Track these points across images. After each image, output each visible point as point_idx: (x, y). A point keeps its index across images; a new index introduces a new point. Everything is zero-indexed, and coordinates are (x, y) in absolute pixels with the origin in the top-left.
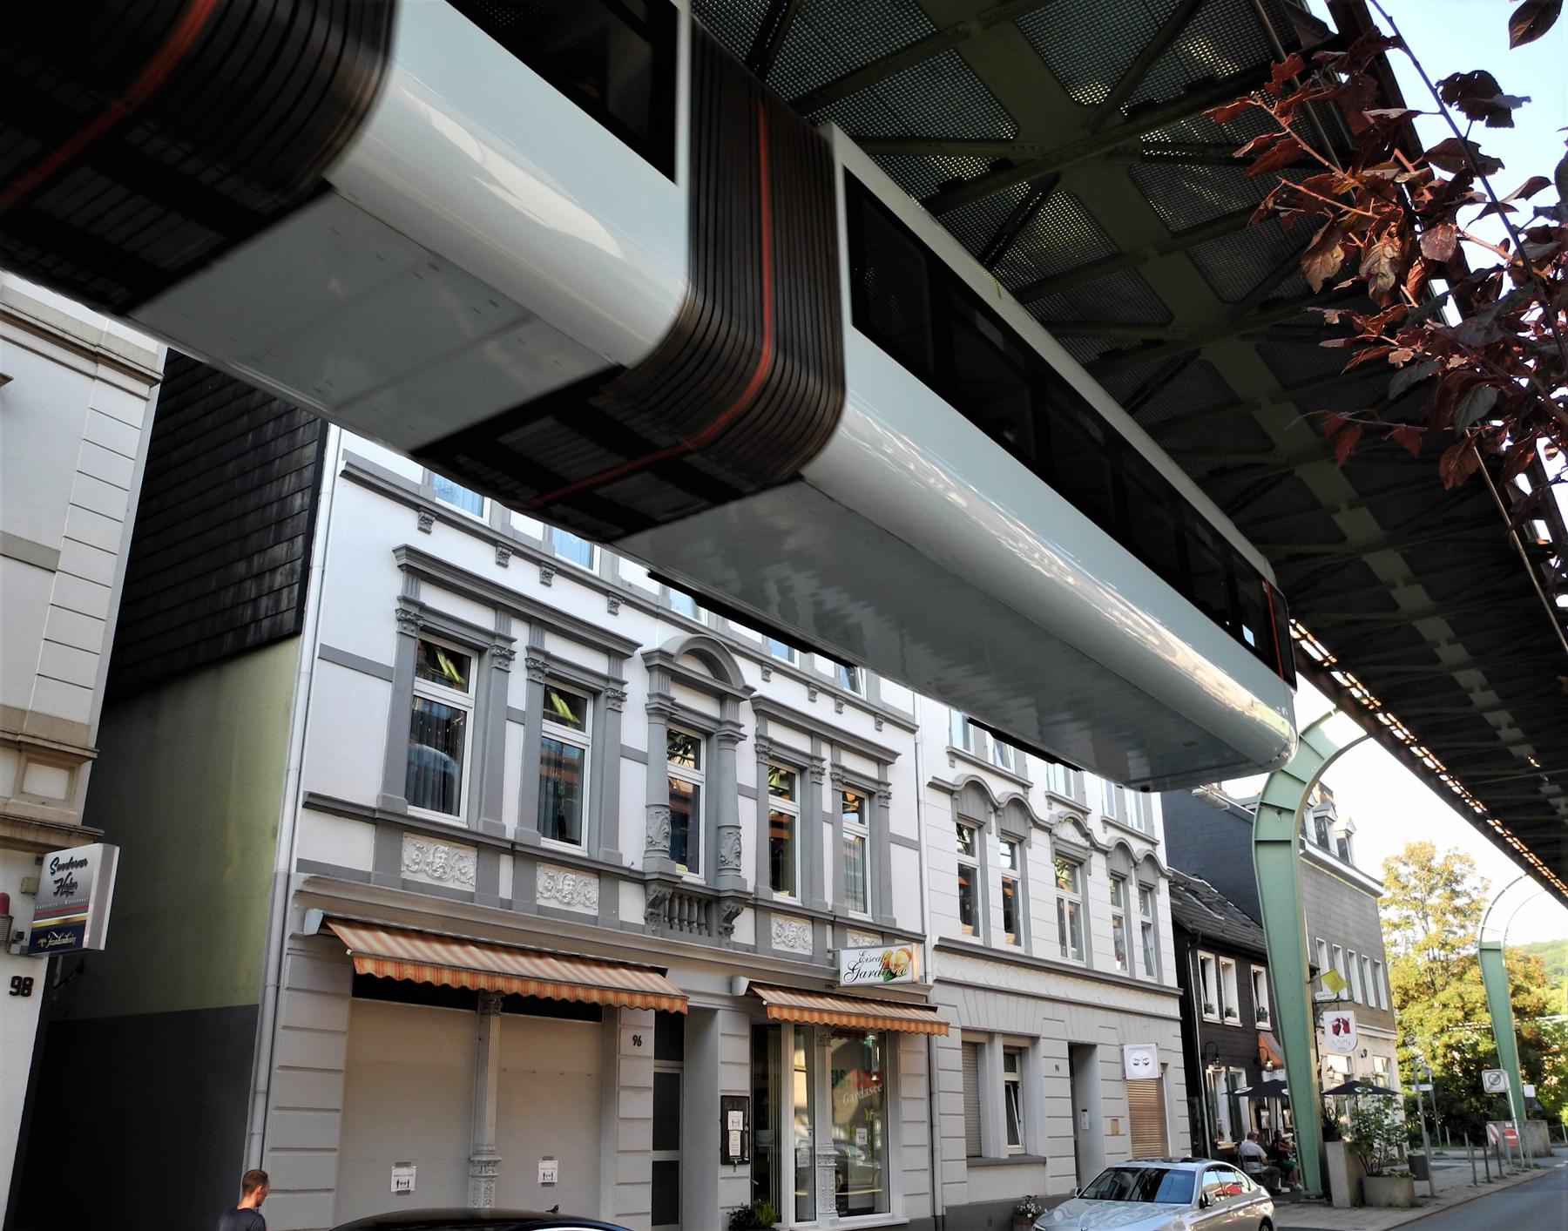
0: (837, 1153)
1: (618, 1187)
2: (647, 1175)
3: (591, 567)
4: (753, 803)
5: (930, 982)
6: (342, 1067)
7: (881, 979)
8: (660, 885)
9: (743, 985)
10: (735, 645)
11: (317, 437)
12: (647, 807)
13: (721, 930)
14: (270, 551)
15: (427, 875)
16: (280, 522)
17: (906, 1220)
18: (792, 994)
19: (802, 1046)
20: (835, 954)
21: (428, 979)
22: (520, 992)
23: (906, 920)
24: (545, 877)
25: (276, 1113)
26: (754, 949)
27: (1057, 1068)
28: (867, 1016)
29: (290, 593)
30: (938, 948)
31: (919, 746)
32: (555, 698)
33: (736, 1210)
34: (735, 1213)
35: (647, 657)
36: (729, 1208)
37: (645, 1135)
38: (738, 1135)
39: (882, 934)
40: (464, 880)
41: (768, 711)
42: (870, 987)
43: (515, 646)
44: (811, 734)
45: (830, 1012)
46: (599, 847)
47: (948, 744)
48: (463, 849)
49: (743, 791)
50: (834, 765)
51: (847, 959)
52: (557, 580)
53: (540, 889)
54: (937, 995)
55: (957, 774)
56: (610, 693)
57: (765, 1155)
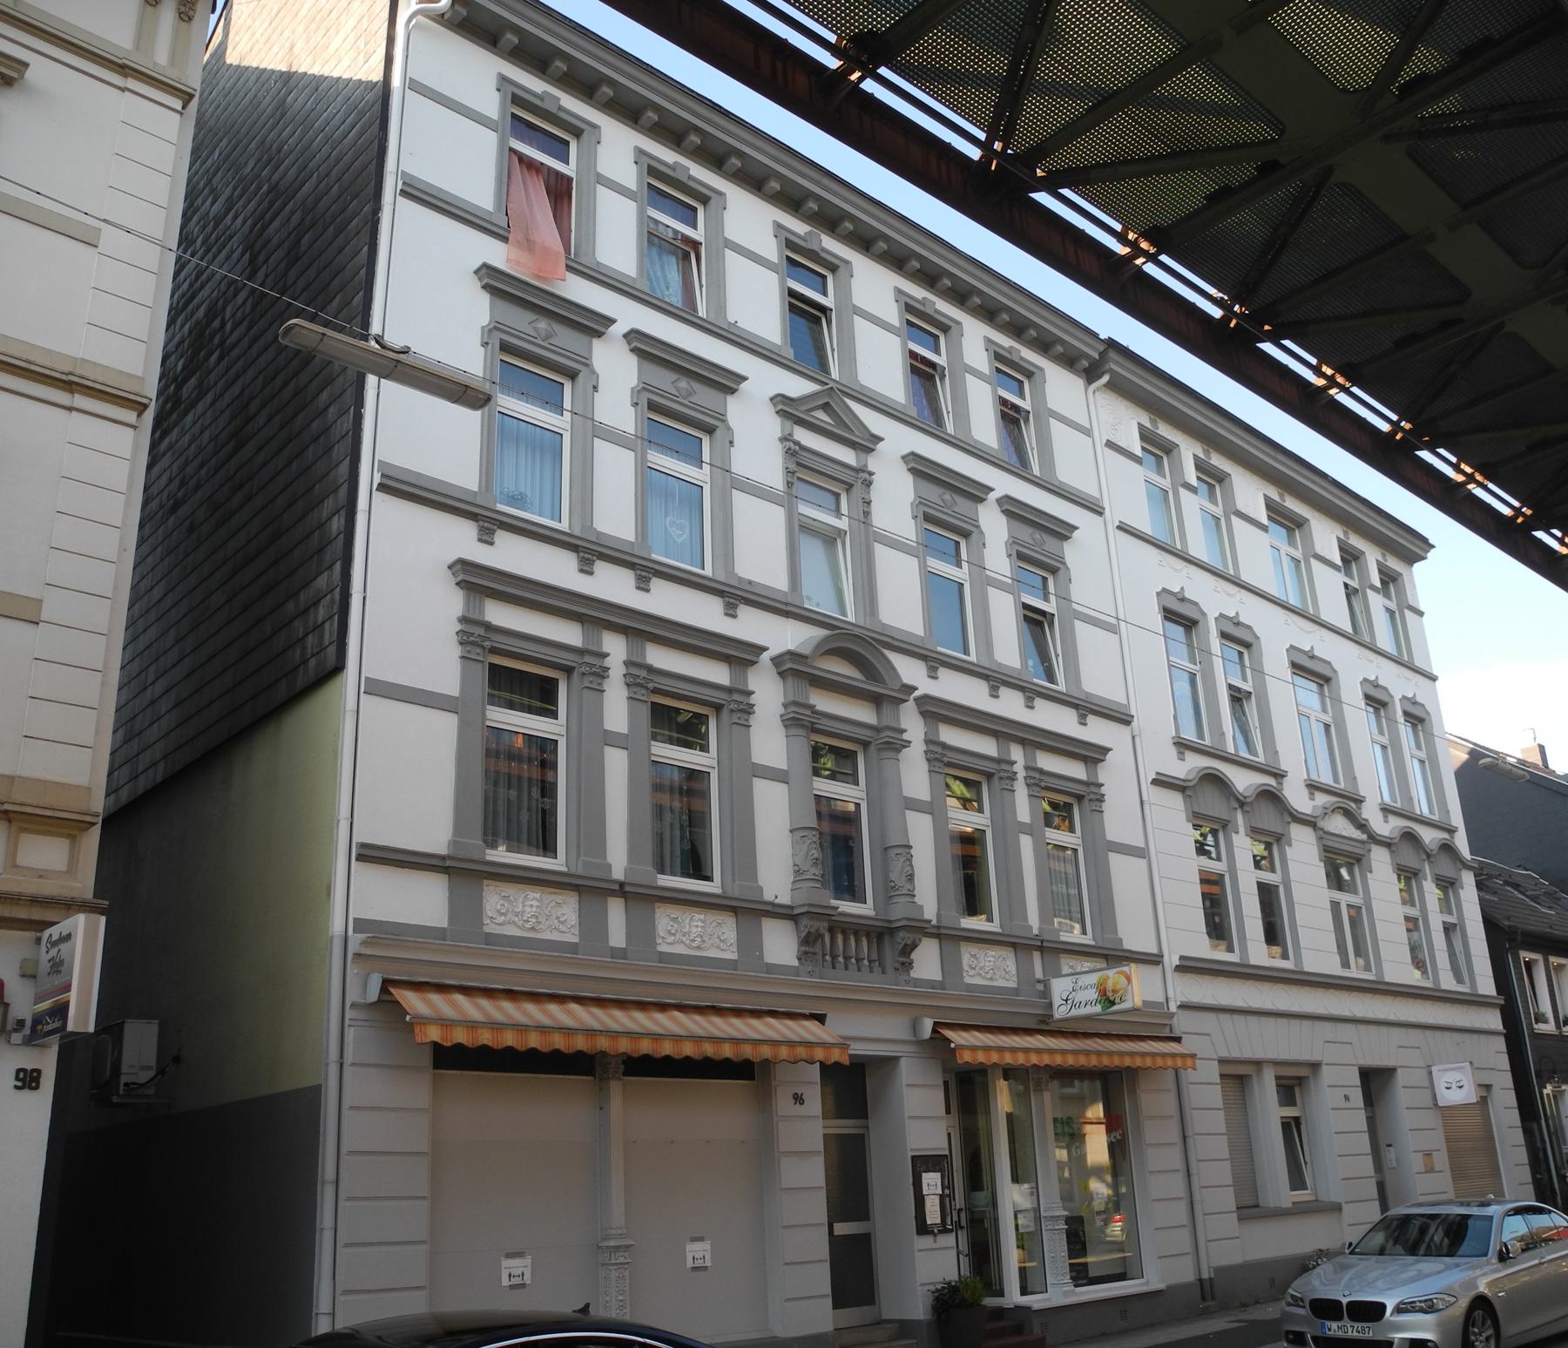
3: (966, 652)
5: (1173, 1008)
7: (1098, 1009)
13: (897, 965)
15: (519, 927)
16: (320, 550)
17: (1161, 1286)
22: (650, 1053)
23: (1134, 937)
24: (666, 920)
26: (941, 985)
27: (1347, 1098)
28: (1087, 1053)
29: (331, 626)
30: (1179, 969)
32: (951, 781)
33: (939, 1287)
34: (937, 1290)
35: (777, 661)
39: (1106, 957)
40: (564, 929)
41: (937, 711)
49: (913, 805)
51: (1060, 987)
55: (1186, 767)
56: (733, 706)
57: (981, 1221)
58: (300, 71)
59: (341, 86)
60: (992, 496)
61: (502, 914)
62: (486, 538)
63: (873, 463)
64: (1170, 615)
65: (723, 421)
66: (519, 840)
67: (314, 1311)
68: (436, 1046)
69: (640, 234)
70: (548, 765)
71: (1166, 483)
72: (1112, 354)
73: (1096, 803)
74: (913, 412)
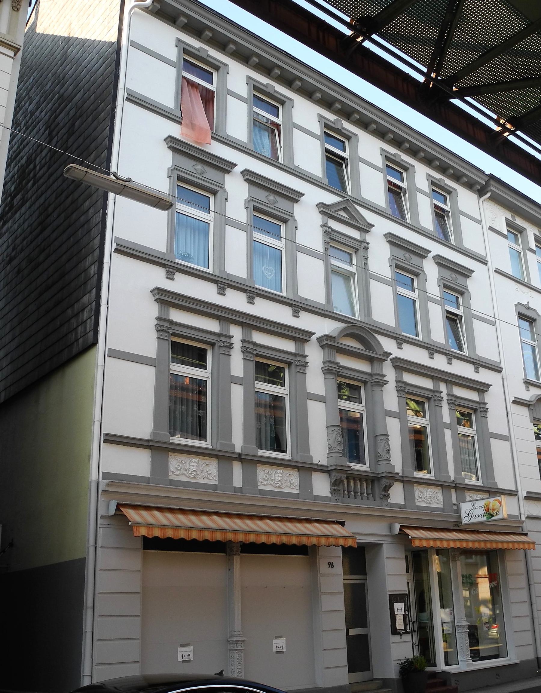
0: (469, 624)
1: (514, 633)
2: (343, 643)
3: (417, 335)
4: (397, 421)
5: (523, 518)
6: (139, 590)
7: (485, 519)
8: (338, 472)
9: (397, 527)
10: (377, 329)
11: (100, 232)
12: (327, 427)
13: (381, 496)
14: (81, 300)
16: (85, 283)
18: (462, 533)
19: (486, 563)
20: (458, 505)
21: (182, 536)
24: (263, 473)
25: (99, 619)
26: (404, 506)
28: (479, 541)
29: (91, 321)
30: (526, 498)
31: (505, 380)
32: (409, 402)
33: (403, 661)
34: (402, 663)
35: (319, 340)
36: (398, 660)
37: (340, 621)
38: (402, 617)
39: (489, 492)
40: (210, 478)
42: (480, 523)
43: (233, 340)
44: (432, 377)
45: (454, 540)
46: (297, 453)
47: (524, 377)
48: (209, 460)
50: (448, 395)
51: (465, 508)
52: (258, 300)
53: (417, 498)
54: (528, 526)
56: (297, 363)
57: (424, 628)
58: (74, 37)
59: (96, 45)
60: (430, 255)
61: (178, 470)
62: (170, 276)
63: (369, 238)
64: (522, 316)
65: (292, 216)
66: (187, 432)
67: (82, 674)
68: (144, 538)
69: (249, 120)
70: (202, 393)
71: (519, 248)
72: (492, 182)
73: (438, 402)
74: (390, 212)
